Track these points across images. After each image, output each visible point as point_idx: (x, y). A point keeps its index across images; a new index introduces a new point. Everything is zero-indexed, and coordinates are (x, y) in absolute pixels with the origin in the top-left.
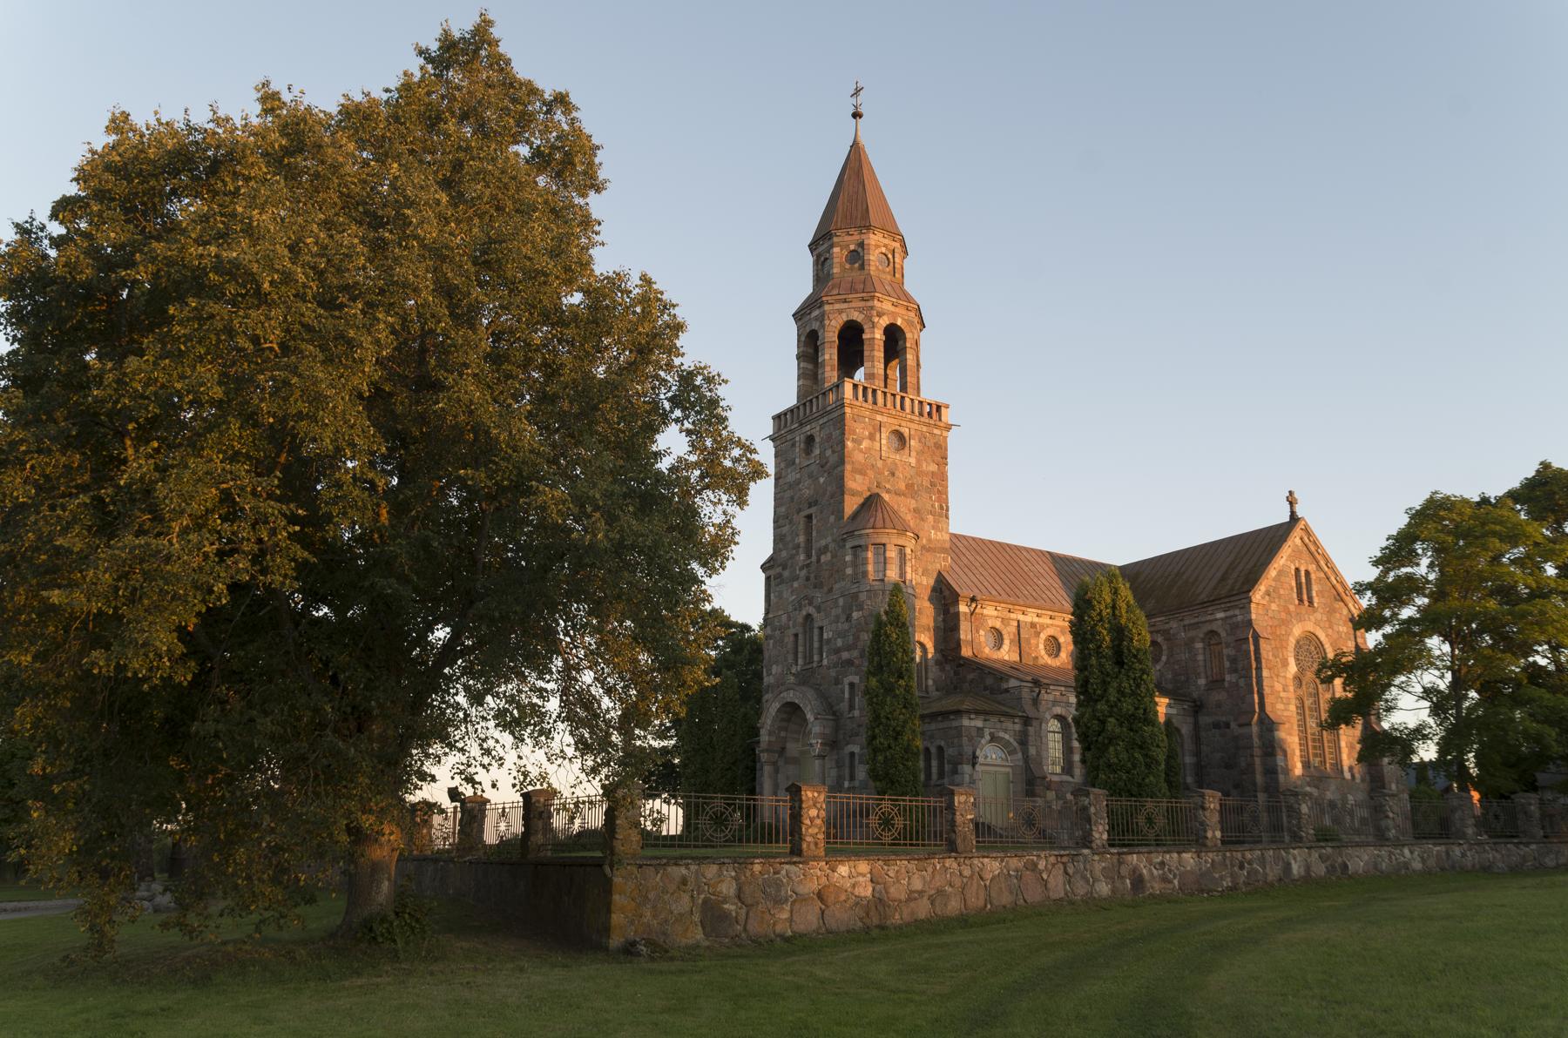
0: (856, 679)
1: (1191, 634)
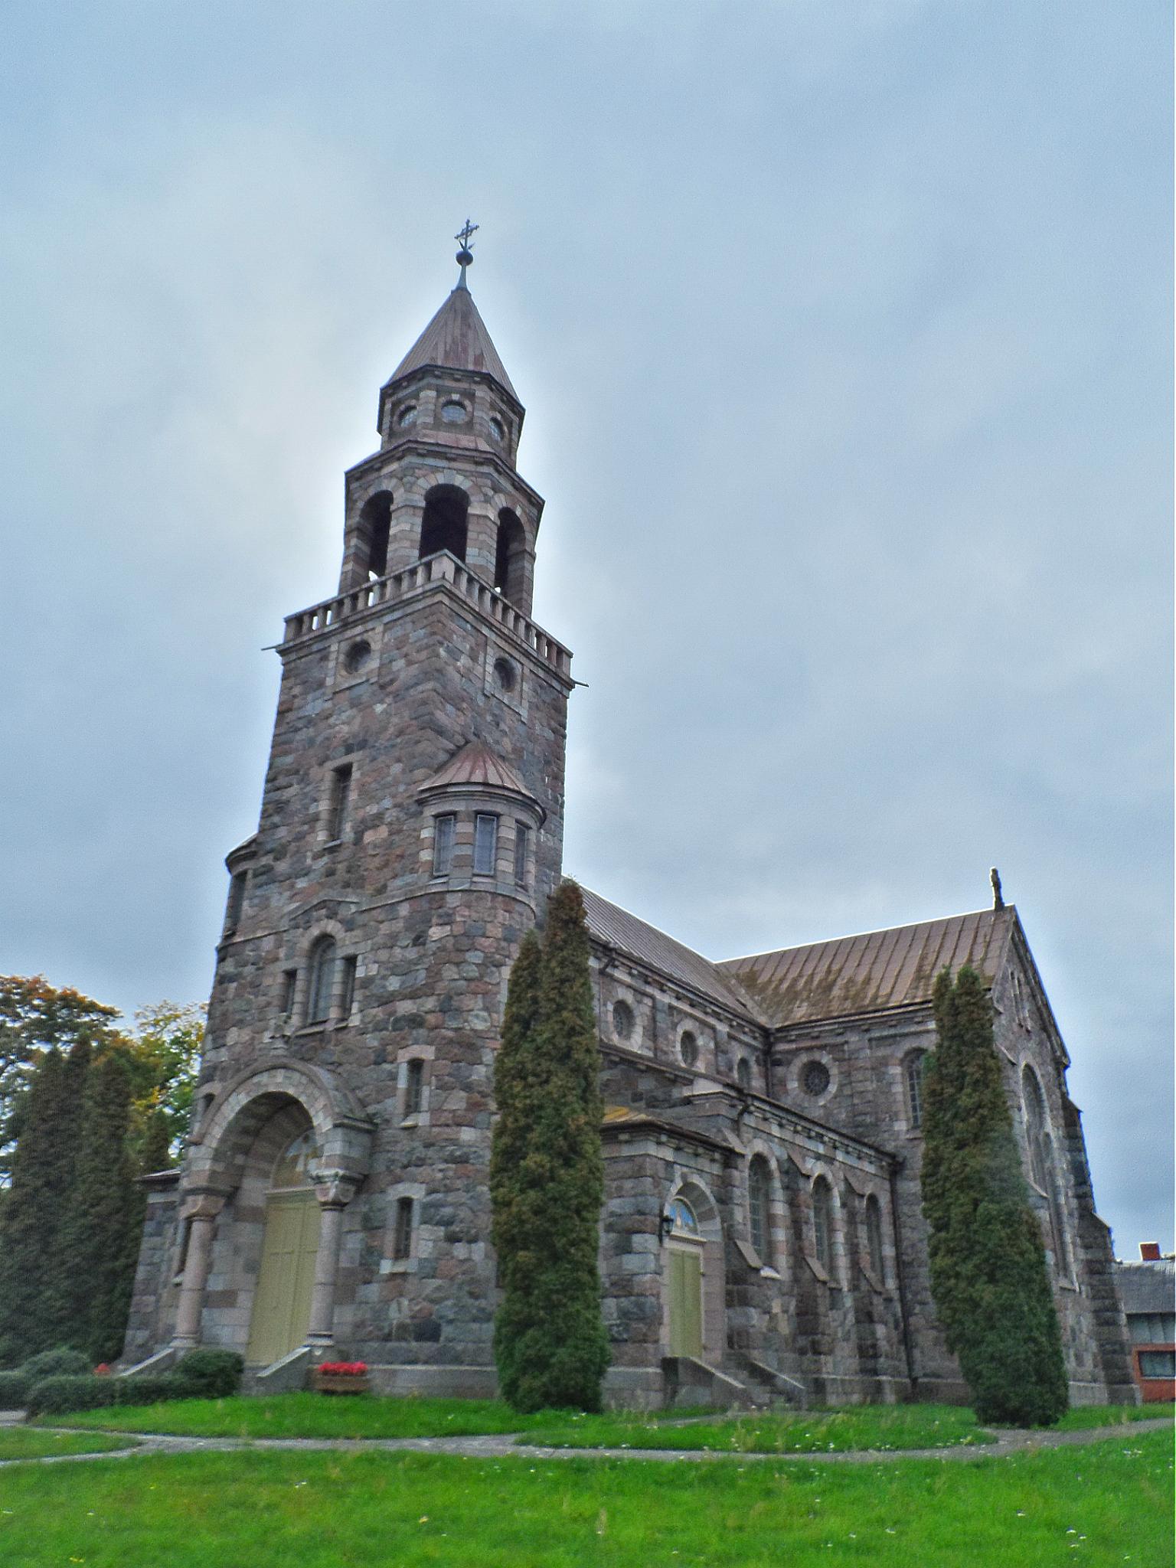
0: (427, 1053)
1: (881, 1052)
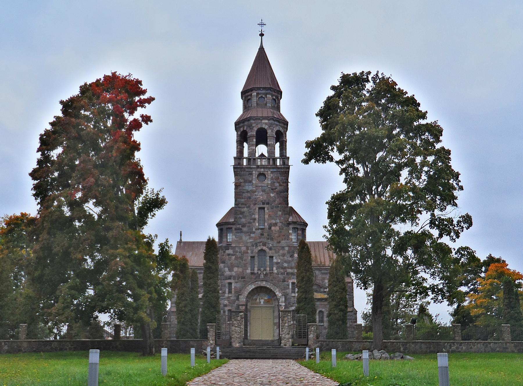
1: (324, 276)
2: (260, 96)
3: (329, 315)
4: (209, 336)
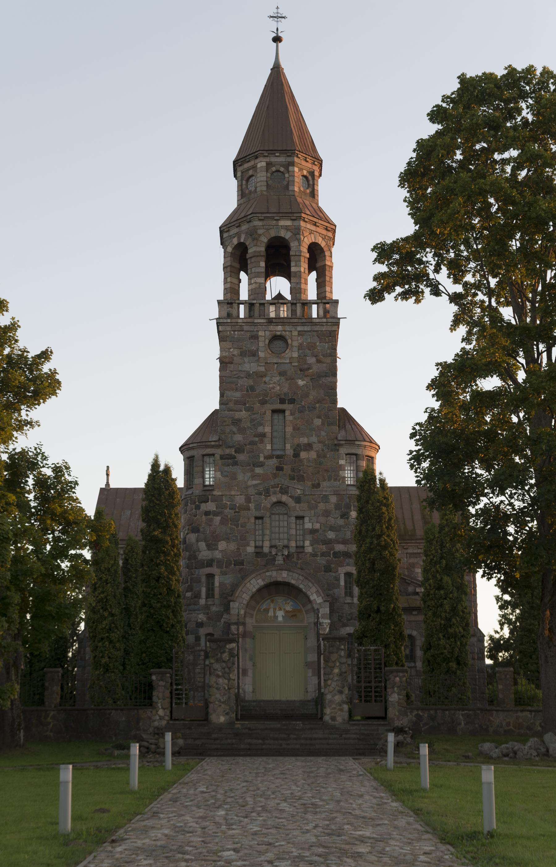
1: (412, 560)
2: (274, 169)
3: (428, 647)
4: (155, 699)
